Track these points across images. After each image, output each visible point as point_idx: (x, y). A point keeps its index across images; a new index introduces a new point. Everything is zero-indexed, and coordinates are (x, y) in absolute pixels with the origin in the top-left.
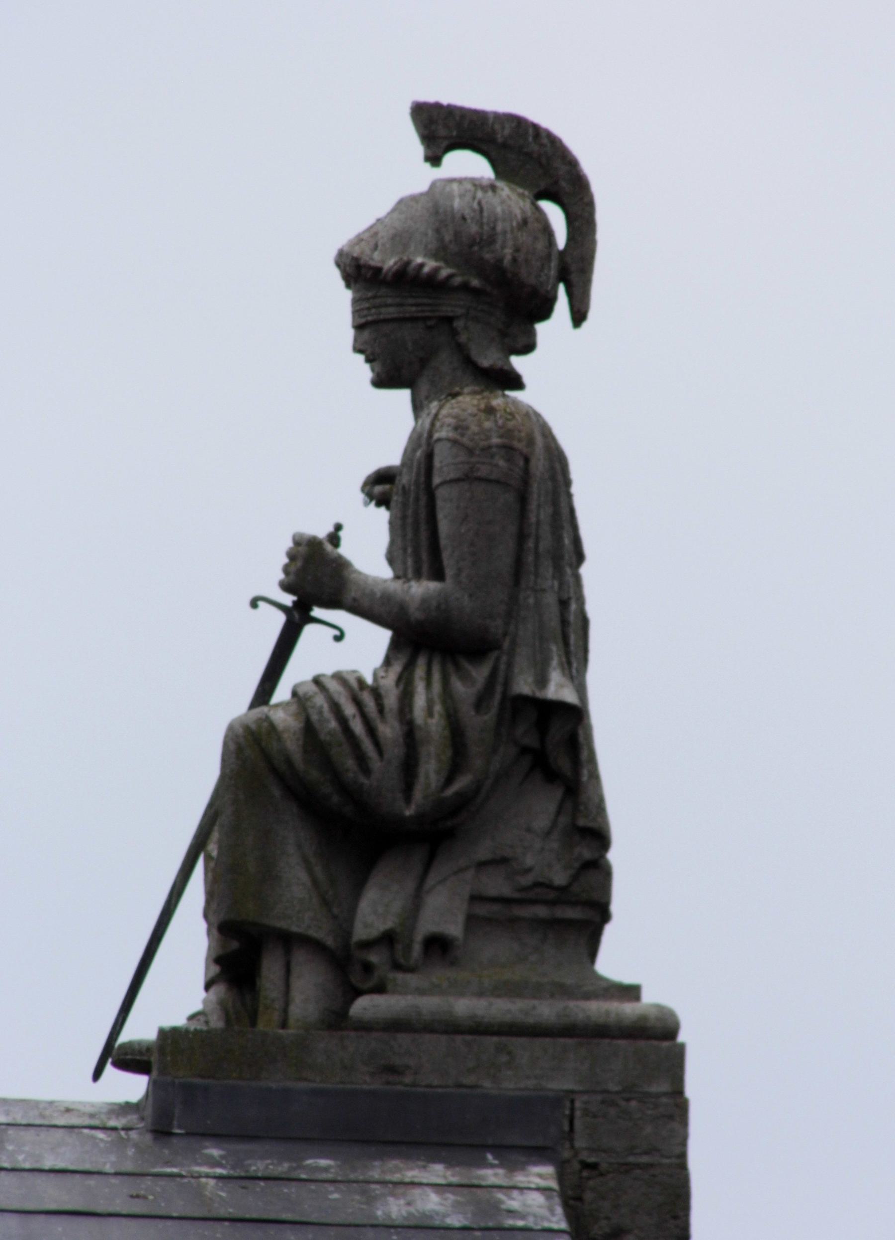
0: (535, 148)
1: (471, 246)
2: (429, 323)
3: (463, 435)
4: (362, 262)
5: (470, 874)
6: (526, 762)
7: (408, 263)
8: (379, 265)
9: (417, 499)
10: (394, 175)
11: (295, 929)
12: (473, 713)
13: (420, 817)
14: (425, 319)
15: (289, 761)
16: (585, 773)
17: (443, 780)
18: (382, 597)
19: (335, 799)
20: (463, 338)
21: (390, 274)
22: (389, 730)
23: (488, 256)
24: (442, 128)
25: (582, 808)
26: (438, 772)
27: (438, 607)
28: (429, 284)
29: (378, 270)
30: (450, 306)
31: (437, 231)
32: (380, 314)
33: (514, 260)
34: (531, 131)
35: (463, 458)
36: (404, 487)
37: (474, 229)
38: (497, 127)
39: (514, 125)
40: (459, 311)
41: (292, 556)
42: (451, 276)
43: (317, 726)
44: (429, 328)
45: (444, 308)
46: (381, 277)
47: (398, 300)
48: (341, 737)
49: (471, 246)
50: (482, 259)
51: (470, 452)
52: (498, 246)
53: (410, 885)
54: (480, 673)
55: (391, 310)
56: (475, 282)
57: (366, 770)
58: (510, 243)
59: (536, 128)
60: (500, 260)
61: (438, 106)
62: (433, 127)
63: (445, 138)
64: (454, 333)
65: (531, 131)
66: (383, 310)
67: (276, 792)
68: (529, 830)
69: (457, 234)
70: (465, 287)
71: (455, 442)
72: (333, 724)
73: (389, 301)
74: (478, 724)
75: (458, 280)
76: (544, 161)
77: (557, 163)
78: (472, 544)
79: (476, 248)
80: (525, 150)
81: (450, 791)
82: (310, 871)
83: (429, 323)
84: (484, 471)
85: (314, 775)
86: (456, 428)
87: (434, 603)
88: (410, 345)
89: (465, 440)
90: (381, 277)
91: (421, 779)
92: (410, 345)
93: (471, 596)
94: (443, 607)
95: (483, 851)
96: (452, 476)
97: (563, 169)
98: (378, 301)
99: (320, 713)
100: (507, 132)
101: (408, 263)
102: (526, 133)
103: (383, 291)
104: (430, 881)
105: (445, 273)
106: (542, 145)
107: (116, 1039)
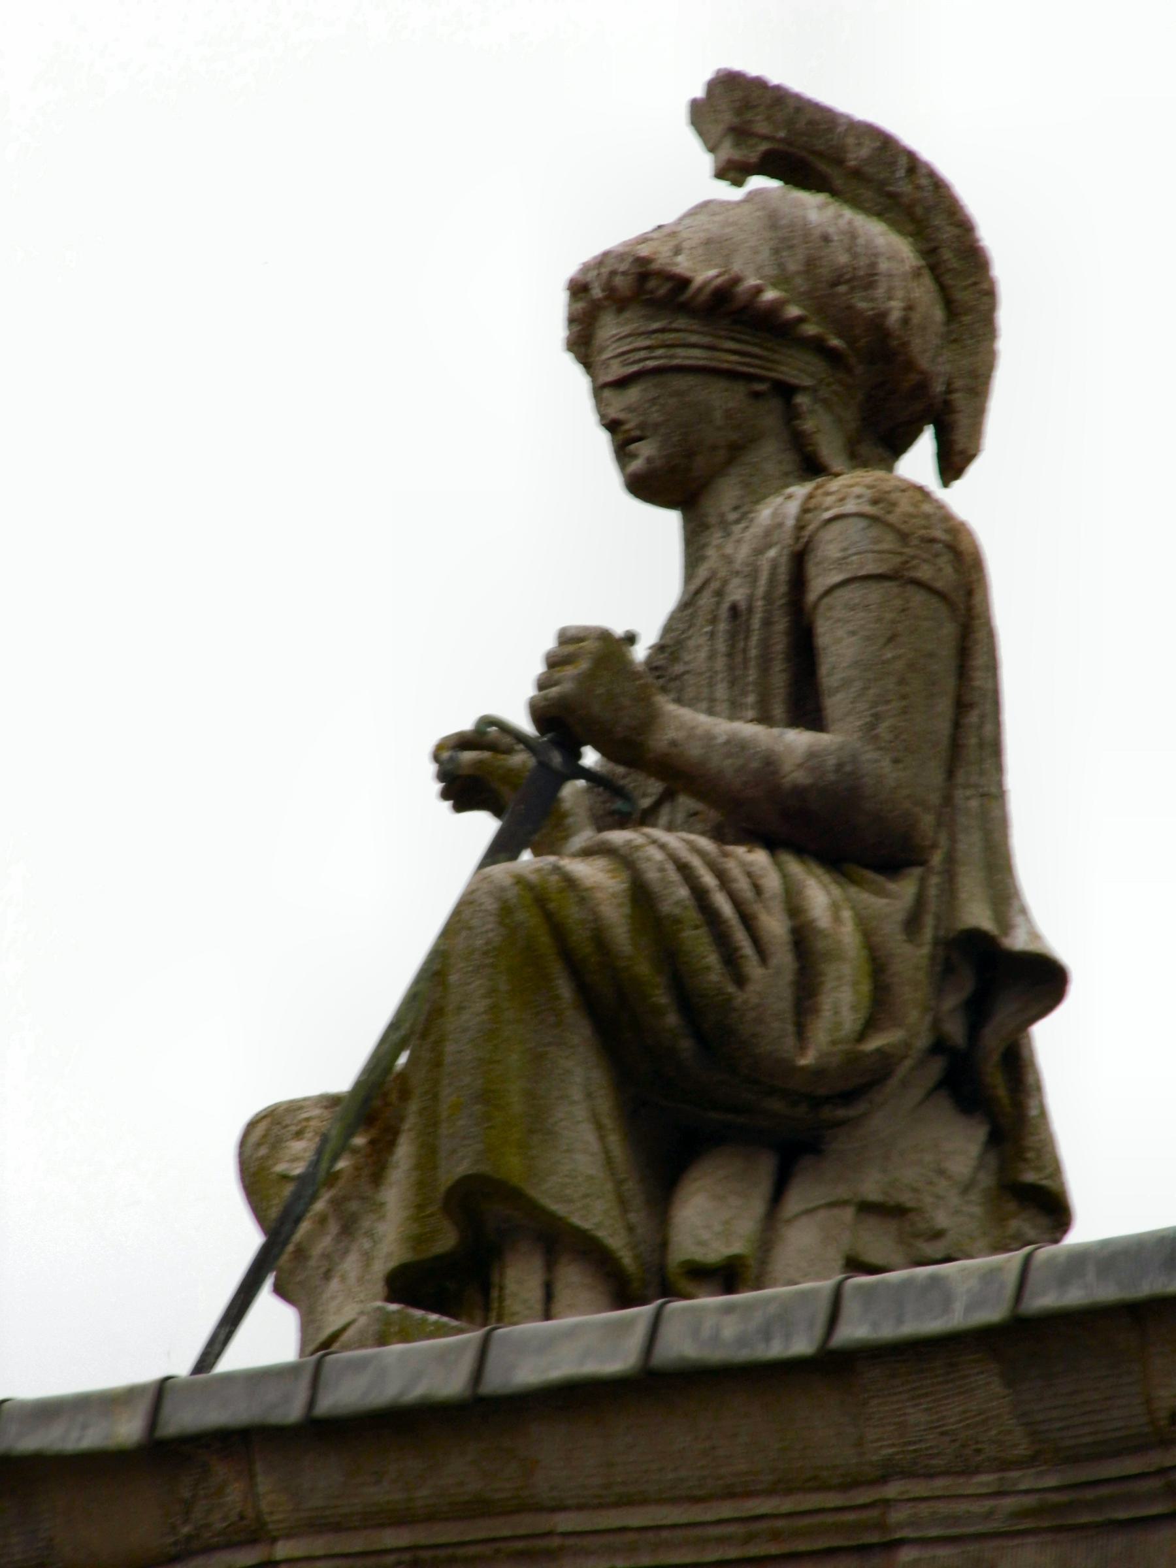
0: (905, 188)
1: (835, 284)
2: (761, 387)
3: (889, 512)
4: (655, 266)
5: (848, 1214)
6: (936, 1068)
7: (737, 280)
8: (688, 274)
9: (767, 623)
10: (662, 184)
11: (576, 1220)
12: (901, 937)
13: (818, 1073)
14: (749, 378)
15: (600, 938)
16: (1033, 1103)
17: (862, 1021)
18: (727, 742)
19: (672, 1019)
20: (808, 425)
21: (708, 290)
22: (775, 925)
23: (862, 305)
24: (758, 127)
25: (1030, 1155)
26: (854, 1008)
27: (839, 766)
28: (765, 324)
29: (683, 283)
30: (797, 368)
31: (776, 251)
32: (672, 357)
33: (905, 321)
34: (903, 161)
35: (889, 542)
36: (734, 610)
37: (843, 258)
38: (850, 141)
39: (878, 144)
40: (807, 382)
41: (555, 662)
42: (801, 320)
43: (657, 888)
44: (757, 395)
45: (784, 368)
46: (683, 298)
47: (706, 340)
48: (693, 915)
49: (835, 284)
50: (850, 307)
51: (904, 537)
52: (880, 292)
53: (758, 1207)
54: (905, 889)
55: (696, 352)
56: (835, 342)
57: (740, 980)
58: (900, 294)
59: (911, 156)
60: (883, 315)
61: (759, 84)
62: (749, 116)
63: (765, 138)
64: (791, 414)
65: (903, 161)
66: (681, 352)
67: (565, 990)
68: (941, 1172)
69: (811, 264)
70: (818, 346)
71: (873, 519)
72: (683, 892)
73: (694, 339)
74: (912, 960)
75: (811, 329)
76: (919, 211)
77: (938, 220)
78: (902, 681)
79: (842, 289)
80: (891, 189)
81: (874, 1043)
82: (602, 1138)
83: (761, 387)
84: (924, 572)
85: (644, 969)
86: (875, 502)
87: (831, 761)
88: (718, 415)
89: (892, 518)
90: (683, 298)
91: (827, 1013)
92: (718, 415)
93: (896, 761)
94: (848, 768)
95: (871, 1188)
96: (871, 568)
97: (948, 233)
98: (670, 337)
99: (662, 870)
100: (865, 152)
101: (737, 280)
102: (893, 164)
103: (681, 322)
104: (793, 1203)
105: (793, 311)
106: (919, 187)
107: (212, 1365)
